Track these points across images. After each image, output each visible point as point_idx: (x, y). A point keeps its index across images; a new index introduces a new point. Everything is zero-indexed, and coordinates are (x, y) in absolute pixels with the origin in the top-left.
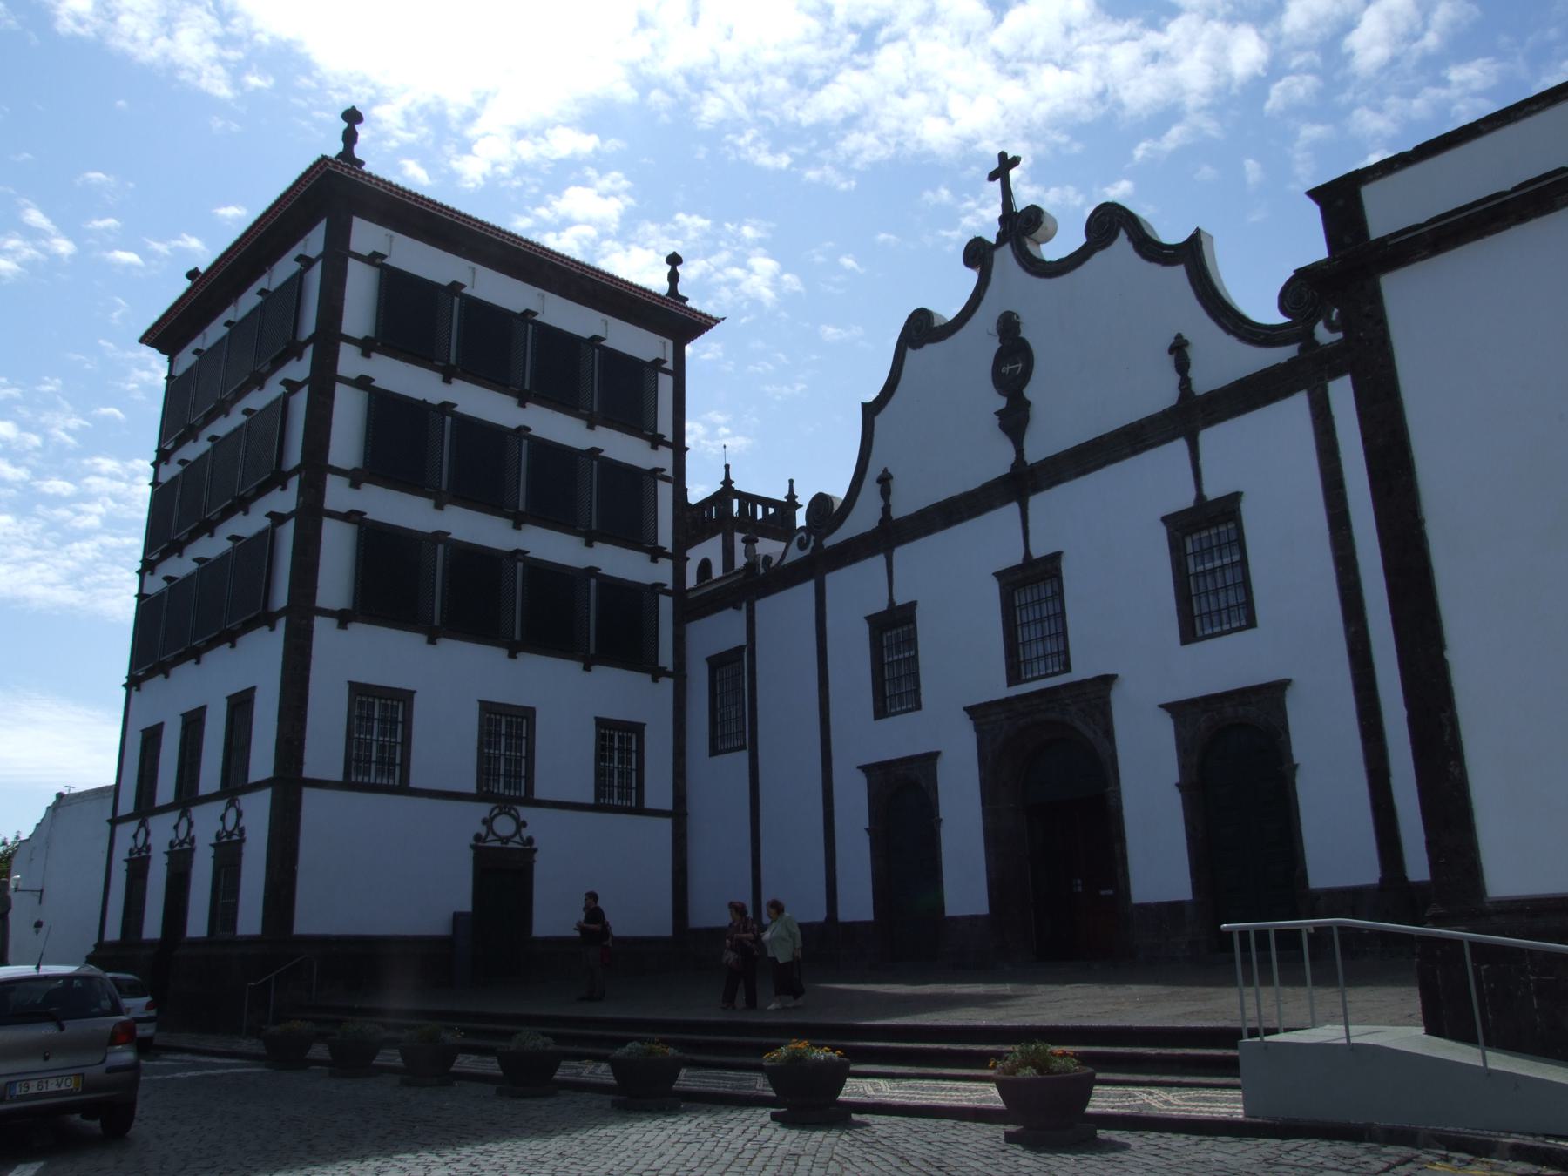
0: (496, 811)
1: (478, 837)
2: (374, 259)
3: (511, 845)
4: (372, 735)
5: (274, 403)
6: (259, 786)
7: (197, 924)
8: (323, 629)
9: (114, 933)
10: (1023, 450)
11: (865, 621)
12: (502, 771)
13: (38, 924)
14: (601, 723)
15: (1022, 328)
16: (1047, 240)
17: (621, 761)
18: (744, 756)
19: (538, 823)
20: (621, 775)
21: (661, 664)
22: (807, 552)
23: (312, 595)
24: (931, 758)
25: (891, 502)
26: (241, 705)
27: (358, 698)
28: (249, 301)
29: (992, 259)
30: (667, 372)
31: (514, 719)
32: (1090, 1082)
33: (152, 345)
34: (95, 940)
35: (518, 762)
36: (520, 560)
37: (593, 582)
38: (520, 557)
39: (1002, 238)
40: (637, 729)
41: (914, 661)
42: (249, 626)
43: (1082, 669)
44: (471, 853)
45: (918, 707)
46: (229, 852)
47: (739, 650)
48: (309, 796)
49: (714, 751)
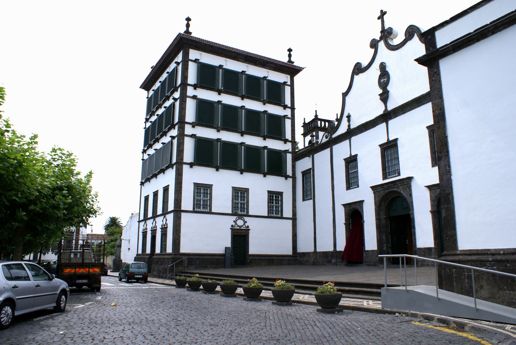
0: (238, 218)
1: (232, 226)
2: (196, 61)
3: (242, 228)
4: (201, 197)
5: (171, 105)
6: (170, 212)
7: (158, 250)
8: (186, 168)
9: (140, 252)
10: (387, 106)
11: (344, 160)
12: (239, 207)
13: (129, 249)
14: (269, 192)
15: (387, 67)
16: (395, 37)
17: (276, 203)
18: (312, 201)
19: (250, 222)
20: (276, 207)
21: (288, 174)
22: (328, 139)
23: (182, 159)
24: (362, 202)
25: (351, 123)
26: (166, 189)
27: (197, 187)
28: (165, 76)
29: (378, 45)
30: (288, 85)
31: (243, 192)
32: (293, 292)
33: (143, 89)
34: (136, 253)
35: (244, 204)
36: (243, 145)
37: (266, 151)
38: (243, 144)
39: (381, 38)
40: (281, 194)
41: (357, 172)
42: (167, 168)
43: (404, 175)
44: (230, 231)
45: (358, 186)
46: (164, 229)
47: (310, 169)
48: (183, 215)
49: (304, 200)
